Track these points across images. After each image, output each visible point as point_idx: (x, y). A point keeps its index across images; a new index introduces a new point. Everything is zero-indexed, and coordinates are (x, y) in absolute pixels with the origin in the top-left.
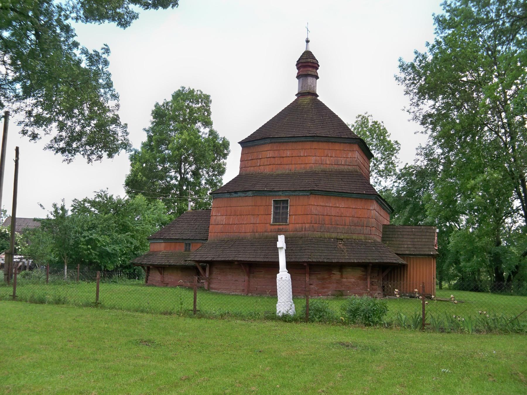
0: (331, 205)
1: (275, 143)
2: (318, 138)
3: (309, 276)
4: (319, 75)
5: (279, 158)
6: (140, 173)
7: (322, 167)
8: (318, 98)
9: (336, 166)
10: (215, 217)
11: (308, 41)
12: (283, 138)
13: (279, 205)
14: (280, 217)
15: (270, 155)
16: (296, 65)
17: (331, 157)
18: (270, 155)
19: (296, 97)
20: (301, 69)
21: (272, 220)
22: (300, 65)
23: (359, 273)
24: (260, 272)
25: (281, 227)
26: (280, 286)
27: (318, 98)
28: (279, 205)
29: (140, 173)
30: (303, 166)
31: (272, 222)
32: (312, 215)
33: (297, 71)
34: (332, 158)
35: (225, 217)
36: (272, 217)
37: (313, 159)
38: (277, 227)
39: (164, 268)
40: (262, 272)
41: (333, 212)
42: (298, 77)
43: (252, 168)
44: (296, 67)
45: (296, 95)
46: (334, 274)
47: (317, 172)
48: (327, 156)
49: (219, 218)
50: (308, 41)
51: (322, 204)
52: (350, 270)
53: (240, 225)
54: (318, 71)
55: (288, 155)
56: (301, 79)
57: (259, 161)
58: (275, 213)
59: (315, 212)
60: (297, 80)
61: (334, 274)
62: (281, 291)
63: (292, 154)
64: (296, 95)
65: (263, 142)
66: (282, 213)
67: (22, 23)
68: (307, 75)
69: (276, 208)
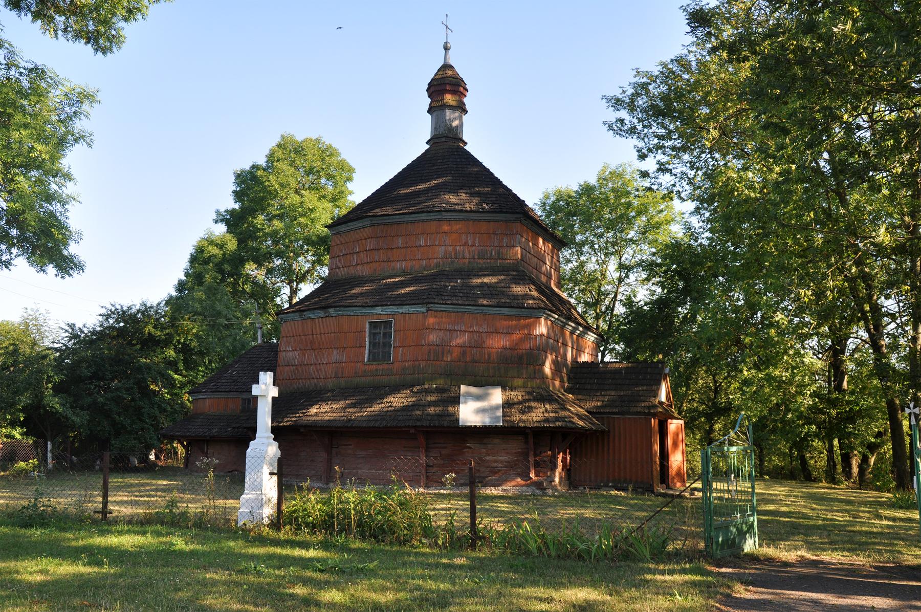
0: (463, 328)
1: (378, 225)
2: (449, 214)
3: (426, 451)
4: (468, 107)
5: (384, 251)
11: (446, 48)
12: (391, 217)
13: (378, 331)
14: (381, 350)
15: (370, 246)
17: (472, 246)
18: (370, 246)
19: (428, 146)
21: (367, 355)
22: (432, 90)
23: (515, 445)
24: (347, 445)
26: (252, 454)
28: (378, 331)
31: (366, 360)
32: (431, 347)
33: (429, 100)
34: (474, 248)
35: (298, 352)
36: (367, 351)
38: (374, 367)
39: (208, 441)
40: (350, 445)
42: (430, 111)
43: (346, 269)
45: (427, 143)
46: (469, 448)
47: (446, 273)
49: (290, 354)
52: (496, 441)
53: (318, 367)
55: (400, 245)
56: (435, 114)
57: (355, 256)
58: (373, 344)
60: (429, 116)
61: (469, 448)
62: (253, 467)
63: (407, 243)
64: (427, 143)
65: (360, 225)
66: (383, 343)
67: (553, 319)
69: (373, 335)
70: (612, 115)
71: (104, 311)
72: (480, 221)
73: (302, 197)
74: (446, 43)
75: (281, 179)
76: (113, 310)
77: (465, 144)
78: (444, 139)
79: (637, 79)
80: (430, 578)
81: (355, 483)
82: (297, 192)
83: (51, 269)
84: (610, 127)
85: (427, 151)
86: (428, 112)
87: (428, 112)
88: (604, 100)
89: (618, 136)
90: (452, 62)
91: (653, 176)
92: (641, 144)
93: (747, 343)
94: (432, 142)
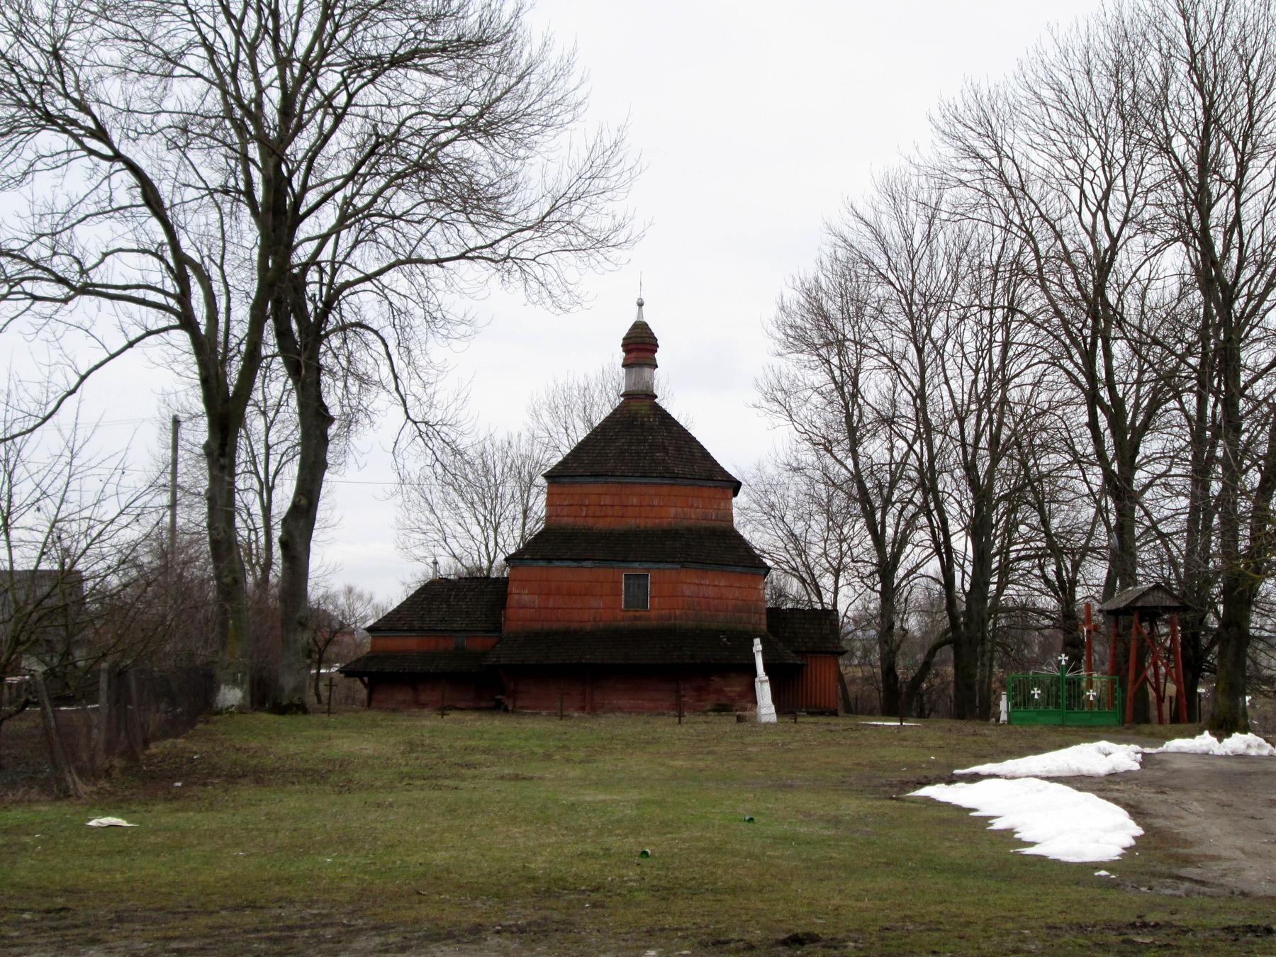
6: (1091, 694)
7: (685, 523)
8: (656, 400)
9: (704, 522)
10: (516, 597)
11: (640, 305)
16: (624, 339)
19: (1133, 842)
20: (634, 354)
25: (638, 614)
27: (656, 400)
29: (1091, 694)
30: (657, 521)
37: (672, 511)
41: (710, 592)
42: (625, 365)
44: (621, 342)
48: (691, 507)
50: (640, 305)
51: (697, 581)
54: (656, 355)
59: (688, 593)
68: (641, 365)
77: (656, 397)
90: (646, 319)
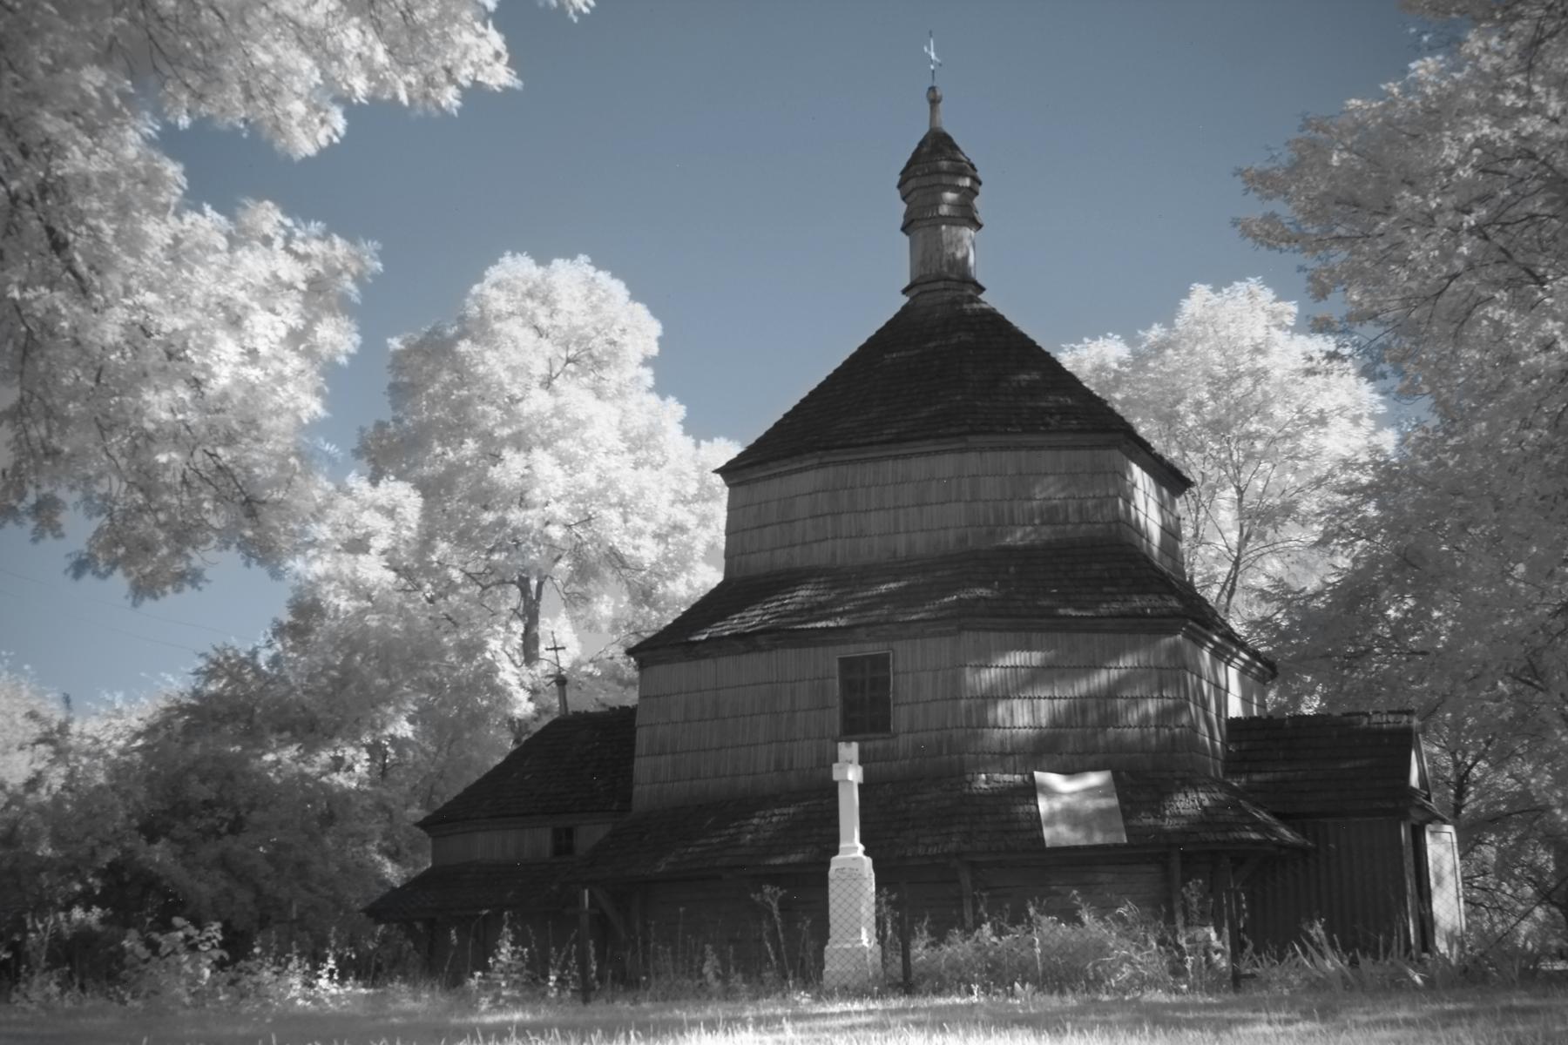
11: (934, 102)
19: (905, 300)
70: (1254, 208)
71: (201, 663)
72: (1041, 448)
73: (557, 396)
74: (932, 89)
75: (515, 358)
76: (221, 659)
78: (941, 285)
79: (1305, 133)
80: (1280, 1022)
81: (601, 978)
82: (547, 383)
83: (187, 588)
84: (1246, 232)
85: (905, 308)
86: (904, 229)
87: (904, 229)
88: (1239, 179)
89: (1264, 249)
91: (1341, 327)
92: (1312, 263)
93: (138, 395)
94: (915, 291)
